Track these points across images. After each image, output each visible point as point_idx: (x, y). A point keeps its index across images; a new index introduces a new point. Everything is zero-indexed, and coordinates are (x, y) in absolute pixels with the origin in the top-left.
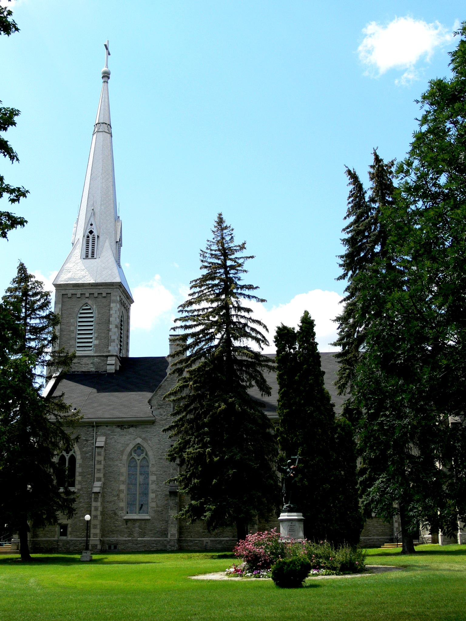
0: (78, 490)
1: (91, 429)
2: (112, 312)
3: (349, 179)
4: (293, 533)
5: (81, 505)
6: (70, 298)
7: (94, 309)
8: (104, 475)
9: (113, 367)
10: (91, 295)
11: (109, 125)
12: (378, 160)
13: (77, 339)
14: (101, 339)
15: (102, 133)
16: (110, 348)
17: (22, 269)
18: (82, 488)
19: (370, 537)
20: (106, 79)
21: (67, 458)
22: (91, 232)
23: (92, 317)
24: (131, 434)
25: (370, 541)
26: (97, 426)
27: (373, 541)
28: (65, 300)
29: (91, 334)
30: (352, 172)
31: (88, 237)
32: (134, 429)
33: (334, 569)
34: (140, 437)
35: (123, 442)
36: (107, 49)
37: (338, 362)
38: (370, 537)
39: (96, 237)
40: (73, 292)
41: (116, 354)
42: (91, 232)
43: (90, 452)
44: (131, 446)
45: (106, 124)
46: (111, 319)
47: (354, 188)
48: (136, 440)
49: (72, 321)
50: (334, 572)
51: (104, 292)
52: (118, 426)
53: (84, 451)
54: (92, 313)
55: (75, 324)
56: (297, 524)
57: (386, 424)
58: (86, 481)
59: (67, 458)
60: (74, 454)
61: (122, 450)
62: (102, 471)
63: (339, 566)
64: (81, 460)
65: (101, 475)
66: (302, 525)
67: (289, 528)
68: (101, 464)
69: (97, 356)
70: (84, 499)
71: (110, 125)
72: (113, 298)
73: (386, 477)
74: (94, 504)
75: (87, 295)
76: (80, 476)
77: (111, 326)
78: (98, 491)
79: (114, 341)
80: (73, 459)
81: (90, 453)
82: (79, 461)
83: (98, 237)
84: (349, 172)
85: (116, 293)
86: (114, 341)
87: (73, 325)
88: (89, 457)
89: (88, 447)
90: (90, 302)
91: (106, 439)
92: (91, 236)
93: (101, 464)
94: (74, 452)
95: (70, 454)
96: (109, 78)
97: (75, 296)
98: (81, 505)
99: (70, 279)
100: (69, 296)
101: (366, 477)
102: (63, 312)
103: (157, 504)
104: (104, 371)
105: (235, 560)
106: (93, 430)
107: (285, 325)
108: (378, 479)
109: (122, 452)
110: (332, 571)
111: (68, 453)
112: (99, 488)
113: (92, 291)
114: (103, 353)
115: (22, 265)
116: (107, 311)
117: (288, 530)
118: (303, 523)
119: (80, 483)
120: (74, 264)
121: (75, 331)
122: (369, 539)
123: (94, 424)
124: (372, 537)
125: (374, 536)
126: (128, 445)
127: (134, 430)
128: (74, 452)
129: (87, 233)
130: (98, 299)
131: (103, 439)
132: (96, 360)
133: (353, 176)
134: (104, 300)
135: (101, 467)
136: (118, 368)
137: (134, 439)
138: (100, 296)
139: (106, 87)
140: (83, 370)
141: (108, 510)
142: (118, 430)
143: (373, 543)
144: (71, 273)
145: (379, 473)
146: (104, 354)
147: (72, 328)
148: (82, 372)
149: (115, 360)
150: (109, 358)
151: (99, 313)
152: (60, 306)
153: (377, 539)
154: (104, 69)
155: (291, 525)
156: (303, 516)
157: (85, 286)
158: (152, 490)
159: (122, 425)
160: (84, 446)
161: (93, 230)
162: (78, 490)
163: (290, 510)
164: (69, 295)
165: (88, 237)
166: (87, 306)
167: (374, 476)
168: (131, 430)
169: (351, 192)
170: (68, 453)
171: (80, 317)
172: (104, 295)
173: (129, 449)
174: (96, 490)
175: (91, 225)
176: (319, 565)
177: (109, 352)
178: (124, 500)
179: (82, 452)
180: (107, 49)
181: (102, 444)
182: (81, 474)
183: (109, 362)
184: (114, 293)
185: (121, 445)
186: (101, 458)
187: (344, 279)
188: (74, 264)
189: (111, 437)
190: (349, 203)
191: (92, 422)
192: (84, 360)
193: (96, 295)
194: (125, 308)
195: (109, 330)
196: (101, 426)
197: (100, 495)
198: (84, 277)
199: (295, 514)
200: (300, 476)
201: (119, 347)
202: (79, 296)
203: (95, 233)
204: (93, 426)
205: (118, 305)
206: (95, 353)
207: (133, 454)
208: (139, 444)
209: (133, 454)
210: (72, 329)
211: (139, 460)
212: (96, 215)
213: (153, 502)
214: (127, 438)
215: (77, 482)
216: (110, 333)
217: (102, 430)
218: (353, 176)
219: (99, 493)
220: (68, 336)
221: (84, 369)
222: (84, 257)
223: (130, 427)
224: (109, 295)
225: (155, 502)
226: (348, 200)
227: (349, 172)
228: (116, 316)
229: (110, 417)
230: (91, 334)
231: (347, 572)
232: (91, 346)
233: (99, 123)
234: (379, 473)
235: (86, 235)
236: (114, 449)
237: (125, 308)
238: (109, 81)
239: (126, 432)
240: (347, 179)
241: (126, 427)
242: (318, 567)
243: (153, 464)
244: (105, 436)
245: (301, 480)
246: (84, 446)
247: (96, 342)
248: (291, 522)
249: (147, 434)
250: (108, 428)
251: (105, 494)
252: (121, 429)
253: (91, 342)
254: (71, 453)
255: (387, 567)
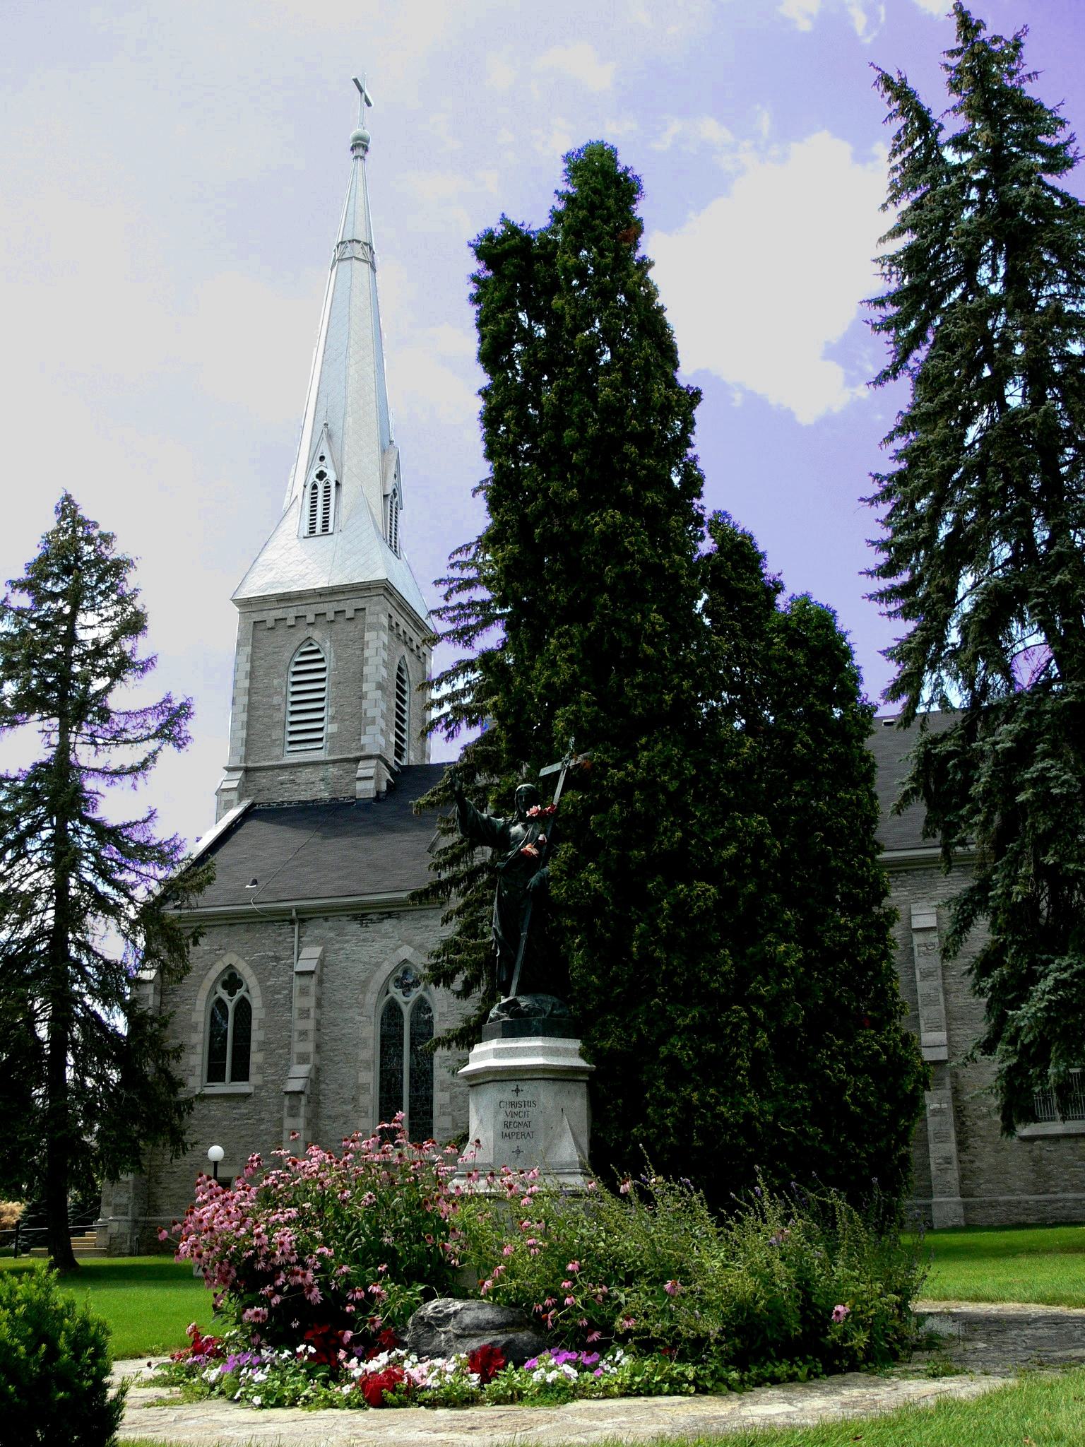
0: (256, 1087)
1: (286, 929)
2: (367, 653)
3: (889, 103)
4: (521, 1143)
5: (262, 1127)
6: (272, 628)
7: (327, 650)
8: (318, 1047)
9: (370, 785)
10: (320, 619)
11: (366, 244)
12: (968, 26)
13: (287, 724)
14: (343, 720)
15: (349, 262)
16: (365, 740)
17: (67, 508)
18: (266, 1083)
19: (1052, 1196)
20: (360, 152)
21: (231, 1006)
22: (321, 475)
23: (323, 670)
24: (385, 936)
25: (1055, 1205)
26: (302, 921)
27: (1063, 1207)
28: (260, 635)
29: (322, 709)
30: (896, 80)
31: (315, 487)
32: (393, 922)
33: (695, 1348)
34: (409, 943)
35: (366, 959)
36: (361, 91)
37: (889, 614)
38: (1052, 1196)
39: (333, 485)
40: (279, 614)
41: (378, 752)
42: (321, 475)
43: (284, 988)
44: (387, 968)
45: (358, 242)
46: (366, 670)
47: (905, 127)
48: (399, 951)
49: (276, 682)
50: (690, 1372)
51: (349, 607)
52: (355, 918)
53: (270, 987)
54: (322, 660)
55: (284, 689)
56: (545, 1095)
57: (1057, 777)
58: (276, 1065)
59: (231, 1006)
60: (246, 995)
61: (363, 978)
62: (311, 1035)
63: (712, 1327)
64: (264, 1010)
65: (309, 1047)
66: (577, 1104)
67: (502, 1117)
68: (308, 1017)
69: (334, 762)
70: (272, 1113)
71: (369, 245)
72: (370, 619)
73: (1070, 966)
74: (288, 1123)
75: (311, 619)
76: (261, 1050)
77: (365, 687)
78: (298, 1089)
79: (373, 721)
80: (244, 1008)
81: (286, 992)
82: (258, 1013)
83: (338, 484)
84: (887, 82)
85: (378, 608)
86: (373, 721)
87: (277, 693)
88: (282, 1002)
89: (279, 975)
90: (316, 634)
91: (324, 952)
92: (321, 485)
93: (308, 1017)
94: (248, 991)
95: (236, 997)
96: (366, 150)
97: (281, 623)
98: (262, 1127)
99: (272, 585)
100: (269, 626)
101: (1001, 974)
102: (257, 663)
103: (454, 1120)
104: (352, 797)
105: (119, 1290)
106: (293, 929)
107: (516, 219)
108: (1046, 976)
109: (365, 984)
110: (676, 1368)
111: (232, 994)
112: (302, 1081)
113: (320, 608)
114: (349, 752)
115: (68, 498)
116: (358, 652)
117: (500, 1127)
118: (585, 1085)
119: (261, 1069)
120: (283, 551)
121: (283, 705)
122: (1051, 1202)
123: (294, 914)
124: (1060, 1196)
125: (1065, 1190)
126: (378, 965)
127: (394, 927)
128: (248, 991)
129: (313, 478)
130: (336, 627)
131: (316, 951)
132: (333, 771)
133: (901, 93)
134: (350, 627)
135: (310, 1025)
136: (384, 787)
137: (395, 950)
138: (340, 619)
139: (360, 170)
140: (302, 798)
141: (331, 1141)
142: (355, 926)
143: (1065, 1212)
144: (274, 572)
145: (1044, 957)
146: (351, 756)
147: (276, 700)
148: (300, 802)
149: (377, 766)
150: (361, 764)
151: (338, 658)
152: (248, 649)
153: (1076, 1200)
154: (357, 131)
155: (512, 1104)
156: (582, 1055)
157: (306, 598)
158: (442, 1082)
159: (364, 915)
160: (270, 974)
161: (325, 471)
162: (256, 1087)
163: (518, 1026)
164: (270, 624)
165: (315, 487)
166: (311, 645)
167: (1029, 969)
168: (387, 925)
169: (898, 138)
170: (232, 994)
171: (295, 673)
172: (349, 614)
173: (380, 976)
174: (294, 1085)
175: (322, 458)
176: (607, 1328)
177: (362, 748)
178: (370, 1111)
179: (265, 990)
180: (361, 91)
181: (311, 966)
182: (264, 1045)
183: (360, 773)
184: (372, 608)
185: (361, 966)
186: (310, 1002)
187: (895, 378)
188: (283, 551)
189: (337, 946)
190: (894, 169)
191: (289, 911)
192: (305, 775)
193: (331, 616)
194: (412, 650)
195: (362, 697)
196: (311, 918)
197: (304, 1099)
198: (303, 577)
199: (537, 1042)
200: (566, 850)
201: (393, 739)
202: (291, 622)
203: (331, 476)
204: (292, 922)
205: (385, 637)
206: (330, 754)
207: (393, 989)
208: (405, 961)
209: (393, 989)
210: (275, 702)
211: (406, 1003)
212: (335, 439)
213: (444, 1114)
214: (377, 946)
215: (253, 1069)
216: (365, 704)
217: (317, 930)
218: (901, 93)
219: (301, 1092)
220: (266, 720)
221: (306, 796)
222: (306, 534)
223: (383, 919)
224: (362, 614)
225: (450, 1114)
226: (890, 160)
227: (887, 82)
228: (379, 660)
229: (333, 893)
230: (322, 709)
231: (782, 1369)
232: (321, 740)
233: (342, 243)
234: (1044, 957)
235: (311, 482)
236: (344, 978)
237: (412, 650)
238: (367, 156)
239: (375, 932)
240: (882, 103)
241: (374, 917)
242: (596, 1336)
243: (442, 1014)
244: (320, 945)
245: (573, 867)
246: (270, 974)
247: (331, 728)
248: (513, 1086)
249: (427, 935)
250: (329, 924)
251: (321, 1098)
252: (362, 924)
253: (321, 729)
254: (240, 993)
255: (1066, 1319)
